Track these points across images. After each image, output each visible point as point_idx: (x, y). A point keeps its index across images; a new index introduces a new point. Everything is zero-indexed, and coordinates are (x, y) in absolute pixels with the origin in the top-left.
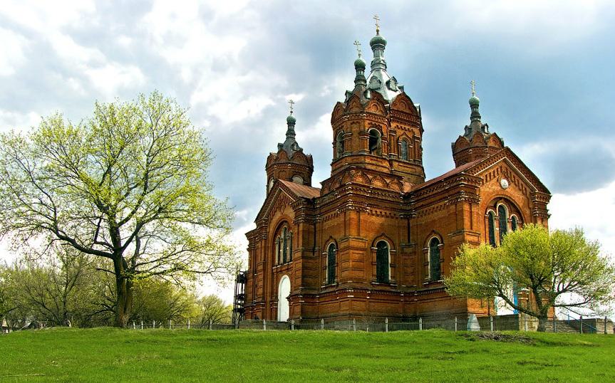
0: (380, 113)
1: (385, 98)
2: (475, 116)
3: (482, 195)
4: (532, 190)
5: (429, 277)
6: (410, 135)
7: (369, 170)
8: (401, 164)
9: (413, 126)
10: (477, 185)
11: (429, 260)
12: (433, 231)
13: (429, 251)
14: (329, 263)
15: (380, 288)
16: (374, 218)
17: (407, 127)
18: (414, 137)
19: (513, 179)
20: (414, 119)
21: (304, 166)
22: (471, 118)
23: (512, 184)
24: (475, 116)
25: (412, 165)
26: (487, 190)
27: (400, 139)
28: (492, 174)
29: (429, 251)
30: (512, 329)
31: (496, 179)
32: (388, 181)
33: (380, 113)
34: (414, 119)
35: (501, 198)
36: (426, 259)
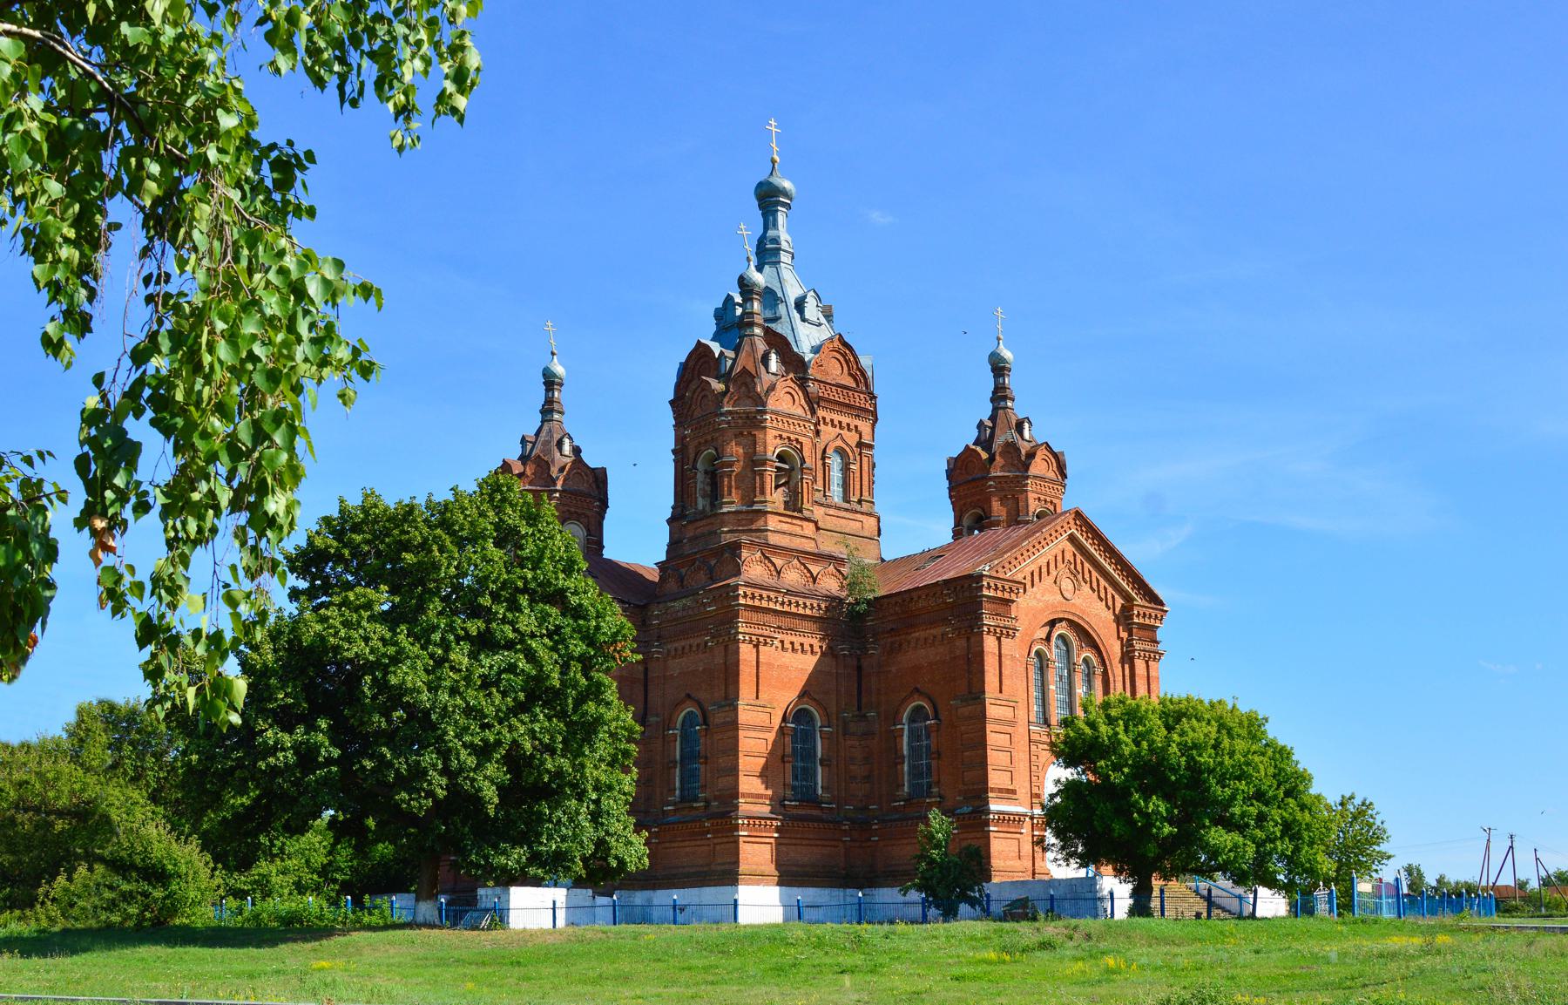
0: (800, 412)
1: (796, 350)
2: (1000, 395)
3: (1022, 617)
4: (1128, 598)
5: (906, 789)
6: (852, 438)
7: (776, 547)
8: (832, 512)
9: (857, 416)
10: (1013, 597)
11: (905, 752)
12: (917, 690)
13: (906, 733)
14: (681, 756)
15: (801, 812)
16: (788, 657)
17: (845, 420)
18: (860, 445)
19: (1087, 576)
20: (860, 400)
21: (589, 495)
22: (992, 400)
23: (1086, 588)
24: (1000, 395)
25: (856, 512)
26: (1032, 606)
27: (830, 452)
28: (1044, 570)
29: (906, 733)
30: (69, 31)
31: (1051, 578)
32: (815, 569)
33: (800, 412)
34: (860, 400)
35: (1061, 620)
36: (896, 750)
